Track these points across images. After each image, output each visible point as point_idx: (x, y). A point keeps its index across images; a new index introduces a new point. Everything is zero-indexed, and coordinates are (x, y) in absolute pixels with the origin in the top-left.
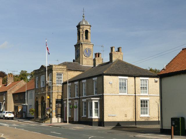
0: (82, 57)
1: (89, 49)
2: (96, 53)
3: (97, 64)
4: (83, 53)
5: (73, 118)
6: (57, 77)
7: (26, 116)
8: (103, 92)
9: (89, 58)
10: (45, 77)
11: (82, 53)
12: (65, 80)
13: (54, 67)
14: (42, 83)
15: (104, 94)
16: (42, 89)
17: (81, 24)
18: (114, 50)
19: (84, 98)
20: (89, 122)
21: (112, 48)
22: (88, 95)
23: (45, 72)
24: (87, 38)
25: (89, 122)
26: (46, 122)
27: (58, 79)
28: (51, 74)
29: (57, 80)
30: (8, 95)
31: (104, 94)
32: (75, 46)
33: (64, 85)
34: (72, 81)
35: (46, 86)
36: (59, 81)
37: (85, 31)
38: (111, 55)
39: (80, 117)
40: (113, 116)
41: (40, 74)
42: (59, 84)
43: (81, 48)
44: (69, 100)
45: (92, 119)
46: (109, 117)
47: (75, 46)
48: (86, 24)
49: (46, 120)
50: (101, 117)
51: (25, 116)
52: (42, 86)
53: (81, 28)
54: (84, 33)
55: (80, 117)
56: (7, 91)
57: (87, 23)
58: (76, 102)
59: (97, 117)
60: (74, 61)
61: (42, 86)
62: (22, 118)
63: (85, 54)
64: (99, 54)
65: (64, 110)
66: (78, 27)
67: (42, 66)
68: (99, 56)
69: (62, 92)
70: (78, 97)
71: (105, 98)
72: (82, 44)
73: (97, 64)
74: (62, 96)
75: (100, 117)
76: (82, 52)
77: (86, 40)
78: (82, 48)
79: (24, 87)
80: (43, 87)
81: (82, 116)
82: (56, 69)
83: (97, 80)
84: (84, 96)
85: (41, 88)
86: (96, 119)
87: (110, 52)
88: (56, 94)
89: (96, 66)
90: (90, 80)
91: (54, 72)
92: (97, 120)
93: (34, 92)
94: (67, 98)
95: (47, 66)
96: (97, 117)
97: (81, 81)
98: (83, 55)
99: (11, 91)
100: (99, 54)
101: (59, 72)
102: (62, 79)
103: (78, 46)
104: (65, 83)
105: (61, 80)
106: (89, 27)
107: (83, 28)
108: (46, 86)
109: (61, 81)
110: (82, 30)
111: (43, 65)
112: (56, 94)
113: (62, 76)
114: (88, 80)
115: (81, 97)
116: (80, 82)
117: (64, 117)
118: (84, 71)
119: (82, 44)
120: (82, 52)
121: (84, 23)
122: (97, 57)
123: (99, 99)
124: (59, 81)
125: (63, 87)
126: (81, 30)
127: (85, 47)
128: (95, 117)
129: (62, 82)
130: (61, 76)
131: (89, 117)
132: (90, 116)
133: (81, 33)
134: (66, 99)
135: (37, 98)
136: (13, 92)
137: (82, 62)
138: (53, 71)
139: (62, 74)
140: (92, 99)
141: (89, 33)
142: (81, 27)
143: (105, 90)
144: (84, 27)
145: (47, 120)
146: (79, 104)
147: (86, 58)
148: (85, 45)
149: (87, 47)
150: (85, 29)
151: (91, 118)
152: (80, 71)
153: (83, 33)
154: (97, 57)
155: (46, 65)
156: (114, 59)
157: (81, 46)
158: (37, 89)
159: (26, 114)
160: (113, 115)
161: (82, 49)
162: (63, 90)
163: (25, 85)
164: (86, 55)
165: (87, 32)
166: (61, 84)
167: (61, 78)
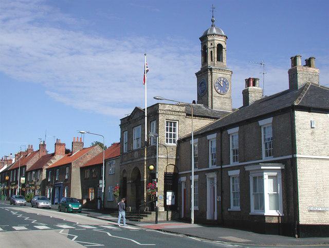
0: (212, 95)
1: (224, 78)
2: (250, 79)
3: (253, 98)
4: (213, 87)
5: (204, 213)
6: (167, 128)
7: (102, 206)
8: (293, 150)
9: (225, 96)
10: (142, 131)
11: (212, 86)
12: (183, 135)
13: (161, 107)
14: (135, 142)
15: (297, 156)
16: (136, 154)
17: (209, 32)
18: (300, 62)
19: (233, 168)
20: (259, 225)
21: (294, 60)
22: (245, 161)
23: (143, 120)
24: (220, 58)
25: (259, 225)
26: (145, 219)
27: (169, 132)
28: (155, 123)
29: (167, 134)
30: (73, 170)
31: (297, 156)
32: (197, 74)
33: (183, 145)
34: (202, 134)
35: (143, 147)
36: (171, 137)
37: (216, 45)
38: (293, 74)
39: (222, 210)
40: (320, 211)
41: (132, 125)
42: (171, 142)
43: (210, 78)
44: (195, 173)
45: (264, 217)
46: (311, 213)
47: (197, 74)
48: (219, 34)
49: (144, 216)
50: (12, 190)
51: (101, 207)
52: (135, 147)
53: (210, 41)
54: (216, 49)
55: (222, 210)
56: (71, 164)
57: (221, 32)
58: (212, 179)
59: (274, 213)
60: (194, 102)
61: (135, 147)
62: (96, 210)
63: (217, 88)
64: (254, 81)
65: (181, 194)
66: (204, 39)
67: (136, 108)
68: (254, 85)
69: (177, 160)
70: (215, 167)
71: (301, 165)
72: (211, 69)
73: (253, 98)
74: (176, 167)
75: (284, 212)
76: (212, 84)
77: (219, 63)
78: (212, 76)
79: (101, 155)
80: (138, 150)
81: (229, 210)
82: (165, 112)
83: (239, 132)
84: (232, 164)
85: (133, 151)
86: (274, 218)
87: (290, 68)
88: (165, 164)
89: (251, 102)
90: (251, 126)
91: (161, 117)
92: (275, 221)
93: (119, 161)
94: (191, 170)
95: (147, 108)
96: (274, 213)
97: (224, 132)
98: (214, 90)
99: (77, 163)
100: (254, 81)
101: (172, 117)
102: (177, 133)
103: (203, 76)
104: (184, 142)
105: (174, 135)
106: (223, 39)
107: (214, 40)
108: (143, 147)
109: (174, 136)
110: (212, 44)
111: (137, 106)
112: (165, 164)
113: (177, 127)
114: (245, 126)
115: (223, 167)
116: (222, 133)
117: (181, 209)
118: (217, 119)
119: (211, 69)
120: (212, 84)
121: (215, 31)
122: (251, 85)
123: (280, 168)
124: (171, 137)
125: (178, 148)
126: (209, 45)
127: (217, 75)
128: (271, 211)
129: (177, 139)
130: (175, 126)
131: (253, 211)
132: (256, 208)
133: (209, 51)
134: (190, 172)
135: (124, 171)
136: (81, 165)
137: (212, 104)
138: (160, 115)
139: (177, 122)
140: (262, 168)
141: (224, 50)
142: (210, 38)
143: (300, 145)
144: (216, 39)
145: (147, 216)
146: (220, 182)
147: (219, 95)
148: (218, 72)
149: (221, 75)
150: (216, 43)
151: (258, 212)
152: (211, 118)
153: (212, 50)
154: (251, 85)
155: (145, 106)
156: (301, 81)
157: (209, 74)
158: (125, 153)
159: (103, 203)
160: (320, 209)
161: (212, 80)
162: (177, 154)
163: (103, 152)
164: (219, 91)
165: (220, 47)
166: (174, 142)
167: (174, 131)
